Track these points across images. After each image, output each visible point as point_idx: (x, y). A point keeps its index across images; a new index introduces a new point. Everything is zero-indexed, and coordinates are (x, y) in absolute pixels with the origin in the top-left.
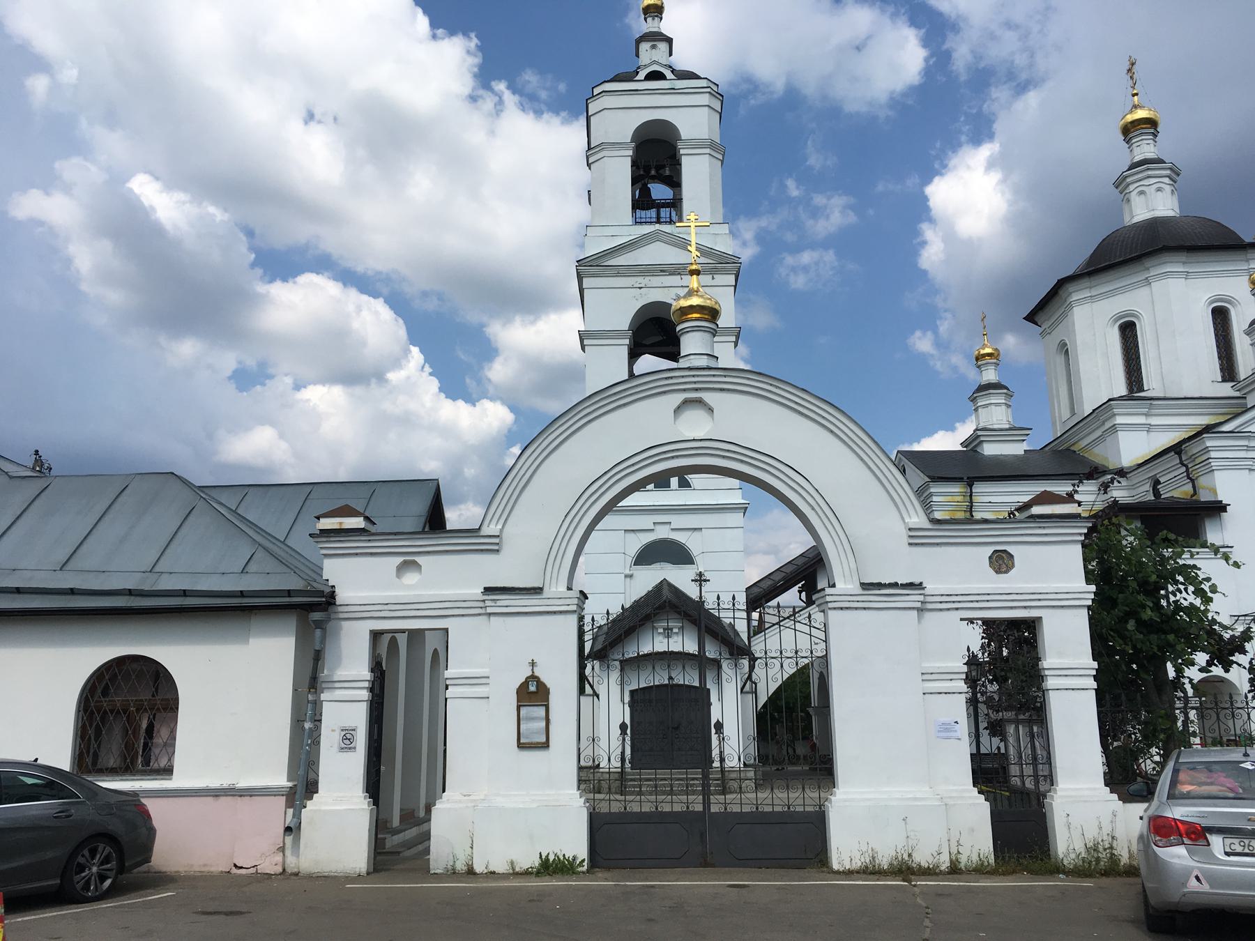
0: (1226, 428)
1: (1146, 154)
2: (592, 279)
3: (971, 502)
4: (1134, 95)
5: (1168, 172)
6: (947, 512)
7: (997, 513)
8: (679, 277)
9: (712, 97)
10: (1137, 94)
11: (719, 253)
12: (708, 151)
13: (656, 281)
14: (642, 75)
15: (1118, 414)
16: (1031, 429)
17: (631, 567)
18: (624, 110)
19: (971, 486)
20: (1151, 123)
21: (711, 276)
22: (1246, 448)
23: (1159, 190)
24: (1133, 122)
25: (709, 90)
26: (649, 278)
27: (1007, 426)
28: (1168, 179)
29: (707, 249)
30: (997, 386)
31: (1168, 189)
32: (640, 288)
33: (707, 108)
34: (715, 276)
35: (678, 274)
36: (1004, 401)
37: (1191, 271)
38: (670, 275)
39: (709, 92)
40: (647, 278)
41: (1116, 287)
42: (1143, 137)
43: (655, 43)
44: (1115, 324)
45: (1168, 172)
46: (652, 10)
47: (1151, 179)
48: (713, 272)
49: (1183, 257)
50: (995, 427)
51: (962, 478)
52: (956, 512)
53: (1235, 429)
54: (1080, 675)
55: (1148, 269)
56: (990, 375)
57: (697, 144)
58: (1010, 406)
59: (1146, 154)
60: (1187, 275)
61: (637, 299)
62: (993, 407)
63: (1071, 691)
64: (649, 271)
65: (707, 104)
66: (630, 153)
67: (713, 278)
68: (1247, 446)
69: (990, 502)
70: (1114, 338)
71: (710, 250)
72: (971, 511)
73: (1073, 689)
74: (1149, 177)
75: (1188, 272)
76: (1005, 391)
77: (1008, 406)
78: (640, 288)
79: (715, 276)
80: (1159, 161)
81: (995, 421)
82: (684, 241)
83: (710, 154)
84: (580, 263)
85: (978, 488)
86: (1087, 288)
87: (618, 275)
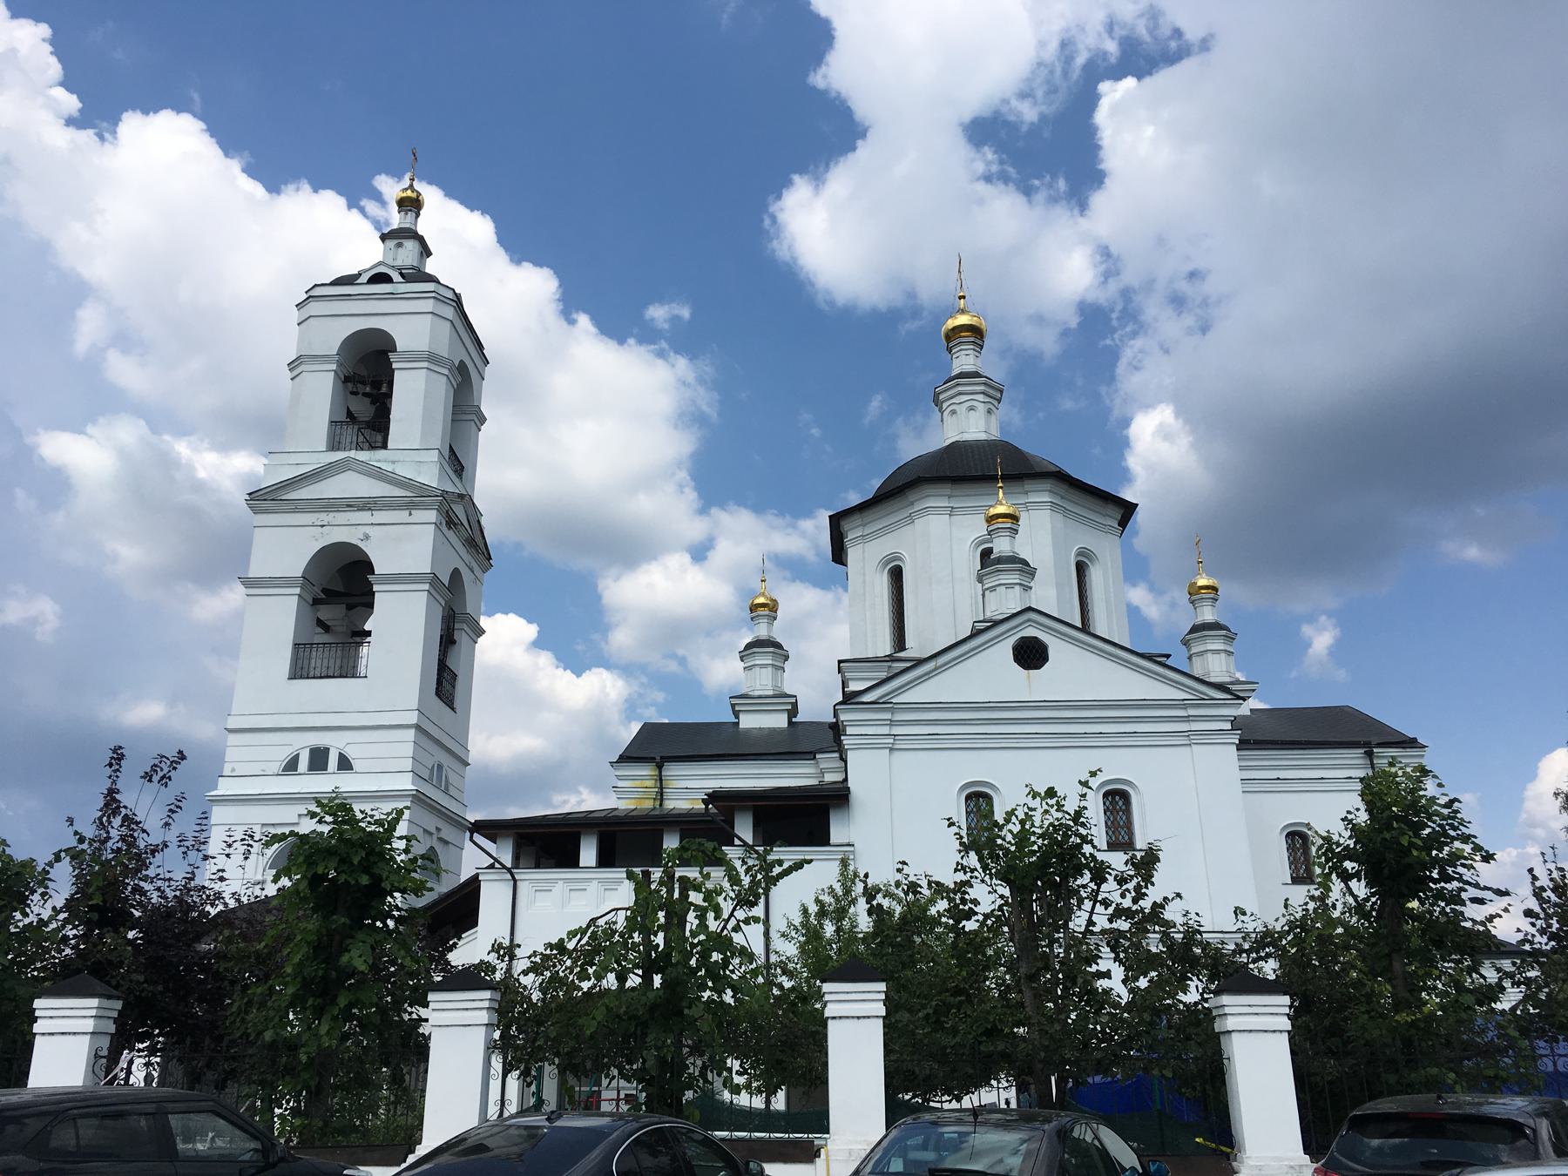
0: (867, 698)
1: (964, 367)
2: (265, 515)
3: (661, 788)
4: (960, 298)
5: (982, 388)
6: (633, 801)
7: (692, 801)
8: (370, 512)
9: (439, 303)
10: (964, 297)
11: (418, 484)
12: (425, 364)
13: (342, 517)
14: (364, 278)
15: (852, 679)
16: (1257, 683)
17: (264, 871)
18: (334, 318)
19: (660, 767)
20: (976, 332)
21: (408, 512)
22: (889, 722)
23: (972, 408)
24: (954, 329)
25: (433, 295)
26: (335, 514)
27: (771, 693)
28: (982, 396)
29: (404, 480)
30: (1216, 626)
31: (981, 408)
32: (322, 526)
33: (430, 315)
34: (413, 512)
35: (369, 509)
36: (770, 662)
37: (955, 506)
38: (358, 510)
39: (434, 298)
40: (332, 515)
41: (885, 525)
42: (962, 347)
43: (401, 241)
44: (883, 573)
45: (982, 388)
46: (406, 204)
47: (961, 396)
48: (410, 506)
49: (946, 489)
50: (757, 693)
51: (654, 758)
52: (643, 800)
53: (1232, 683)
54: (63, 1017)
55: (912, 503)
56: (1207, 614)
57: (413, 357)
58: (1232, 653)
59: (964, 367)
60: (952, 511)
61: (316, 540)
62: (1209, 655)
63: (856, 1020)
64: (333, 506)
65: (431, 311)
66: (334, 367)
67: (410, 514)
68: (890, 720)
69: (687, 788)
70: (883, 583)
71: (407, 481)
72: (662, 800)
73: (858, 1018)
74: (960, 394)
75: (952, 508)
76: (1224, 632)
77: (1229, 653)
78: (322, 526)
79: (413, 512)
80: (976, 375)
81: (758, 687)
82: (378, 470)
83: (428, 368)
84: (252, 496)
85: (673, 771)
86: (859, 526)
87: (295, 511)
